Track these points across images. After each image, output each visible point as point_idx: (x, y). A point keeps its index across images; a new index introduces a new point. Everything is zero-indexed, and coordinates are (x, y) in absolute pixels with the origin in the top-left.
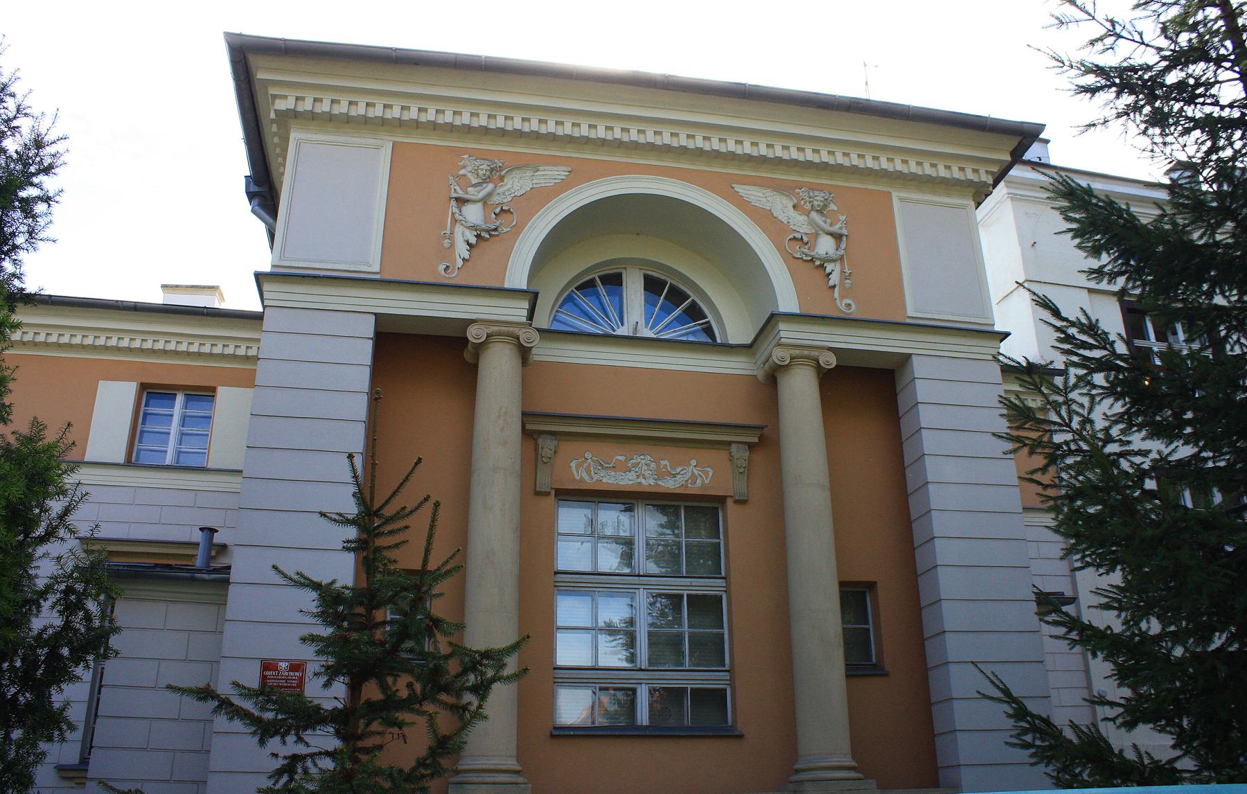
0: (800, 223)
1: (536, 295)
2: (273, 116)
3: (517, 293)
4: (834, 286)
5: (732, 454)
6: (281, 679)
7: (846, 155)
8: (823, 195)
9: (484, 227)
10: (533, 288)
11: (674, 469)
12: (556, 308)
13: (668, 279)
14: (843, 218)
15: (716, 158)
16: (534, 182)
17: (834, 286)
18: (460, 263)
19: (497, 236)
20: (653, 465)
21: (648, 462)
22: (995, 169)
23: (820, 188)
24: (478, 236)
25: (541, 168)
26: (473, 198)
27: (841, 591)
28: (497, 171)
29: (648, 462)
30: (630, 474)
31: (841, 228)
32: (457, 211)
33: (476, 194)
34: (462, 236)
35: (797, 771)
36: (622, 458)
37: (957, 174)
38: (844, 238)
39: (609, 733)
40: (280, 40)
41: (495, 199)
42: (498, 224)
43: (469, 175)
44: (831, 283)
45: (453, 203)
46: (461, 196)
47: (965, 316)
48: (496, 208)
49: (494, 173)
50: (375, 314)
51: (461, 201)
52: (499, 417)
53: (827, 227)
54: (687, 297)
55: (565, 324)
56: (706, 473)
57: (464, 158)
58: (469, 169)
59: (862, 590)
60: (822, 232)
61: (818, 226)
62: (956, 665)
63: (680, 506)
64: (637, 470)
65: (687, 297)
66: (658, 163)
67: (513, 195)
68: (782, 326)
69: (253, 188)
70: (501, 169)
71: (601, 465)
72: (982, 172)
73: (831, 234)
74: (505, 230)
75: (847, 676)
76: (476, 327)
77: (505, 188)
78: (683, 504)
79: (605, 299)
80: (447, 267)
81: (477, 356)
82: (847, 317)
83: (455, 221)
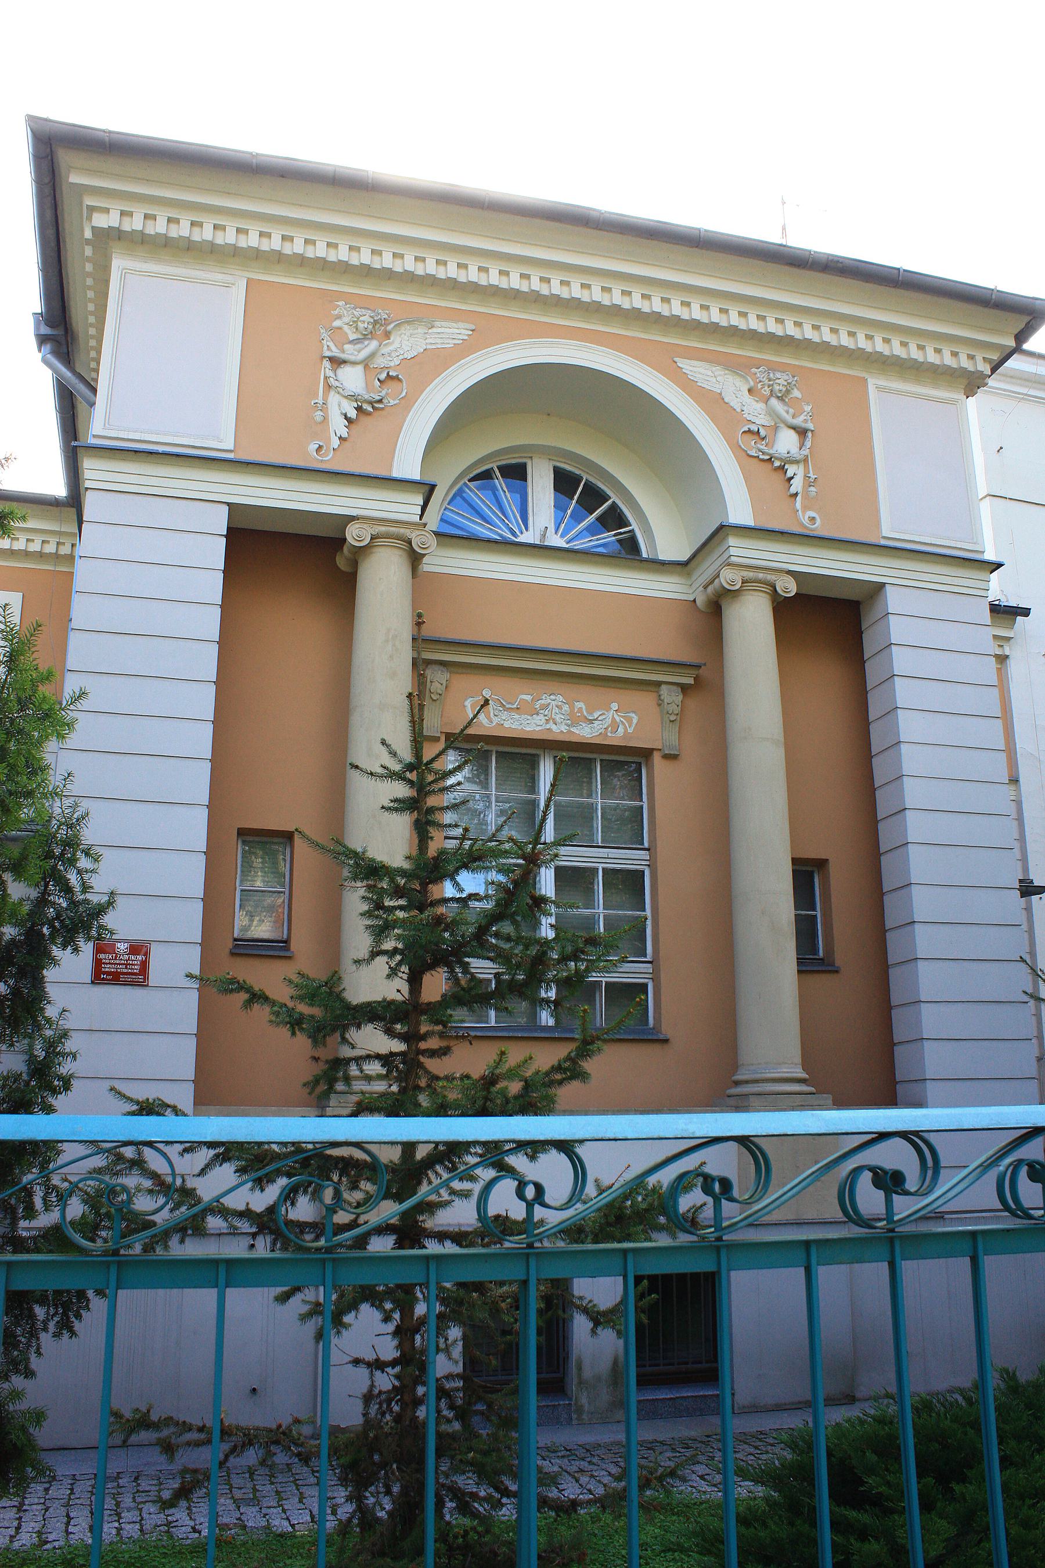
0: (756, 413)
1: (432, 487)
2: (88, 234)
3: (302, 472)
4: (796, 494)
5: (662, 698)
6: (119, 964)
7: (780, 321)
8: (786, 378)
9: (366, 397)
10: (430, 479)
11: (591, 714)
12: (445, 504)
13: (583, 474)
14: (808, 408)
15: (733, 335)
16: (429, 341)
17: (796, 494)
18: (335, 443)
19: (382, 409)
20: (566, 707)
21: (560, 703)
22: (995, 357)
23: (783, 368)
24: (359, 409)
25: (437, 324)
26: (352, 358)
27: (793, 871)
28: (381, 325)
29: (560, 703)
30: (539, 718)
31: (806, 421)
32: (331, 374)
33: (356, 353)
34: (338, 408)
35: (737, 1083)
36: (528, 698)
37: (948, 360)
38: (809, 434)
39: (511, 1034)
40: (104, 131)
41: (380, 362)
42: (383, 393)
43: (346, 328)
44: (793, 490)
45: (326, 364)
46: (336, 354)
47: (949, 539)
48: (380, 373)
49: (378, 326)
50: (228, 504)
51: (337, 362)
52: (387, 641)
53: (789, 419)
54: (606, 498)
55: (462, 529)
56: (630, 720)
57: (339, 306)
58: (346, 319)
59: (809, 869)
60: (782, 425)
61: (779, 417)
62: (926, 963)
63: (492, 751)
64: (546, 713)
65: (606, 498)
66: (700, 346)
67: (401, 357)
68: (732, 541)
69: (45, 330)
70: (387, 322)
71: (503, 705)
72: (979, 358)
73: (794, 428)
74: (392, 402)
75: (799, 971)
76: (357, 526)
77: (391, 348)
78: (494, 748)
79: (506, 496)
80: (320, 447)
81: (355, 564)
82: (811, 533)
83: (329, 387)
